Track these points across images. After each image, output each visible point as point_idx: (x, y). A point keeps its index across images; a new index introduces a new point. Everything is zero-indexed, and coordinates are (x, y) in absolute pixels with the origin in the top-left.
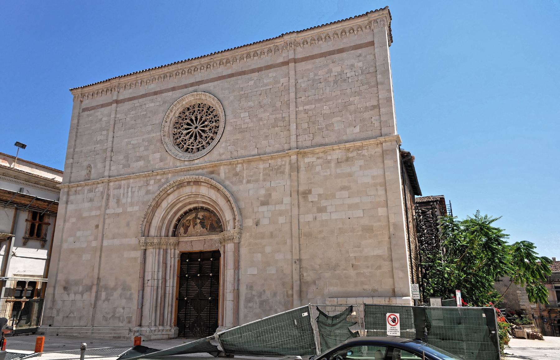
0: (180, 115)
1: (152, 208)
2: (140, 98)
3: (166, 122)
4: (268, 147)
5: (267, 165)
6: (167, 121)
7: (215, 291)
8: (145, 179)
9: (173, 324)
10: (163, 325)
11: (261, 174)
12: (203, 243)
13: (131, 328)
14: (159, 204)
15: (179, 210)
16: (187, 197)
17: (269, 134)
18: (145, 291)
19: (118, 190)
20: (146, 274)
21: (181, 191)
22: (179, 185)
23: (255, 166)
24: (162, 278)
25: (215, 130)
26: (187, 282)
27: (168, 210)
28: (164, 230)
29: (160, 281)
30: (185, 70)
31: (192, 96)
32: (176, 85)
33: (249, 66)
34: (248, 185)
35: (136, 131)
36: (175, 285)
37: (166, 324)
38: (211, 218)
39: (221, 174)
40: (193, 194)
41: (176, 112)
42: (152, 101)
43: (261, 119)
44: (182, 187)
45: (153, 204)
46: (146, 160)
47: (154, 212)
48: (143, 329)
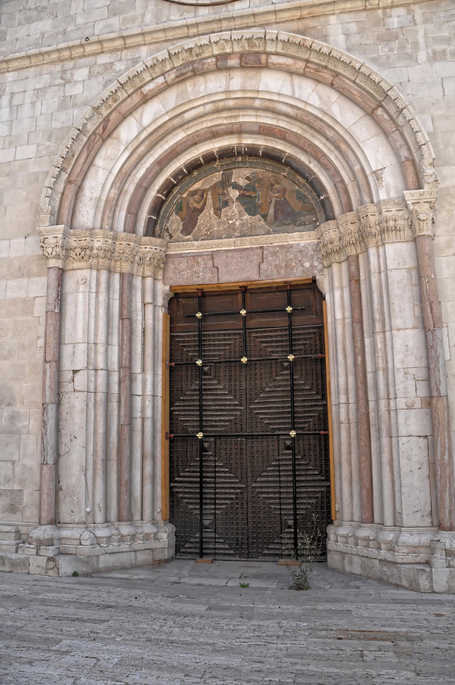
1: (85, 139)
7: (305, 412)
8: (58, 68)
9: (159, 517)
10: (130, 520)
12: (256, 259)
13: (23, 530)
14: (110, 126)
16: (209, 107)
18: (65, 407)
20: (67, 350)
21: (189, 89)
22: (184, 66)
24: (120, 367)
26: (201, 380)
27: (142, 149)
28: (123, 213)
29: (115, 378)
34: (438, 65)
36: (160, 392)
37: (137, 517)
38: (278, 183)
40: (233, 96)
45: (91, 127)
46: (60, 17)
47: (92, 153)
48: (66, 533)
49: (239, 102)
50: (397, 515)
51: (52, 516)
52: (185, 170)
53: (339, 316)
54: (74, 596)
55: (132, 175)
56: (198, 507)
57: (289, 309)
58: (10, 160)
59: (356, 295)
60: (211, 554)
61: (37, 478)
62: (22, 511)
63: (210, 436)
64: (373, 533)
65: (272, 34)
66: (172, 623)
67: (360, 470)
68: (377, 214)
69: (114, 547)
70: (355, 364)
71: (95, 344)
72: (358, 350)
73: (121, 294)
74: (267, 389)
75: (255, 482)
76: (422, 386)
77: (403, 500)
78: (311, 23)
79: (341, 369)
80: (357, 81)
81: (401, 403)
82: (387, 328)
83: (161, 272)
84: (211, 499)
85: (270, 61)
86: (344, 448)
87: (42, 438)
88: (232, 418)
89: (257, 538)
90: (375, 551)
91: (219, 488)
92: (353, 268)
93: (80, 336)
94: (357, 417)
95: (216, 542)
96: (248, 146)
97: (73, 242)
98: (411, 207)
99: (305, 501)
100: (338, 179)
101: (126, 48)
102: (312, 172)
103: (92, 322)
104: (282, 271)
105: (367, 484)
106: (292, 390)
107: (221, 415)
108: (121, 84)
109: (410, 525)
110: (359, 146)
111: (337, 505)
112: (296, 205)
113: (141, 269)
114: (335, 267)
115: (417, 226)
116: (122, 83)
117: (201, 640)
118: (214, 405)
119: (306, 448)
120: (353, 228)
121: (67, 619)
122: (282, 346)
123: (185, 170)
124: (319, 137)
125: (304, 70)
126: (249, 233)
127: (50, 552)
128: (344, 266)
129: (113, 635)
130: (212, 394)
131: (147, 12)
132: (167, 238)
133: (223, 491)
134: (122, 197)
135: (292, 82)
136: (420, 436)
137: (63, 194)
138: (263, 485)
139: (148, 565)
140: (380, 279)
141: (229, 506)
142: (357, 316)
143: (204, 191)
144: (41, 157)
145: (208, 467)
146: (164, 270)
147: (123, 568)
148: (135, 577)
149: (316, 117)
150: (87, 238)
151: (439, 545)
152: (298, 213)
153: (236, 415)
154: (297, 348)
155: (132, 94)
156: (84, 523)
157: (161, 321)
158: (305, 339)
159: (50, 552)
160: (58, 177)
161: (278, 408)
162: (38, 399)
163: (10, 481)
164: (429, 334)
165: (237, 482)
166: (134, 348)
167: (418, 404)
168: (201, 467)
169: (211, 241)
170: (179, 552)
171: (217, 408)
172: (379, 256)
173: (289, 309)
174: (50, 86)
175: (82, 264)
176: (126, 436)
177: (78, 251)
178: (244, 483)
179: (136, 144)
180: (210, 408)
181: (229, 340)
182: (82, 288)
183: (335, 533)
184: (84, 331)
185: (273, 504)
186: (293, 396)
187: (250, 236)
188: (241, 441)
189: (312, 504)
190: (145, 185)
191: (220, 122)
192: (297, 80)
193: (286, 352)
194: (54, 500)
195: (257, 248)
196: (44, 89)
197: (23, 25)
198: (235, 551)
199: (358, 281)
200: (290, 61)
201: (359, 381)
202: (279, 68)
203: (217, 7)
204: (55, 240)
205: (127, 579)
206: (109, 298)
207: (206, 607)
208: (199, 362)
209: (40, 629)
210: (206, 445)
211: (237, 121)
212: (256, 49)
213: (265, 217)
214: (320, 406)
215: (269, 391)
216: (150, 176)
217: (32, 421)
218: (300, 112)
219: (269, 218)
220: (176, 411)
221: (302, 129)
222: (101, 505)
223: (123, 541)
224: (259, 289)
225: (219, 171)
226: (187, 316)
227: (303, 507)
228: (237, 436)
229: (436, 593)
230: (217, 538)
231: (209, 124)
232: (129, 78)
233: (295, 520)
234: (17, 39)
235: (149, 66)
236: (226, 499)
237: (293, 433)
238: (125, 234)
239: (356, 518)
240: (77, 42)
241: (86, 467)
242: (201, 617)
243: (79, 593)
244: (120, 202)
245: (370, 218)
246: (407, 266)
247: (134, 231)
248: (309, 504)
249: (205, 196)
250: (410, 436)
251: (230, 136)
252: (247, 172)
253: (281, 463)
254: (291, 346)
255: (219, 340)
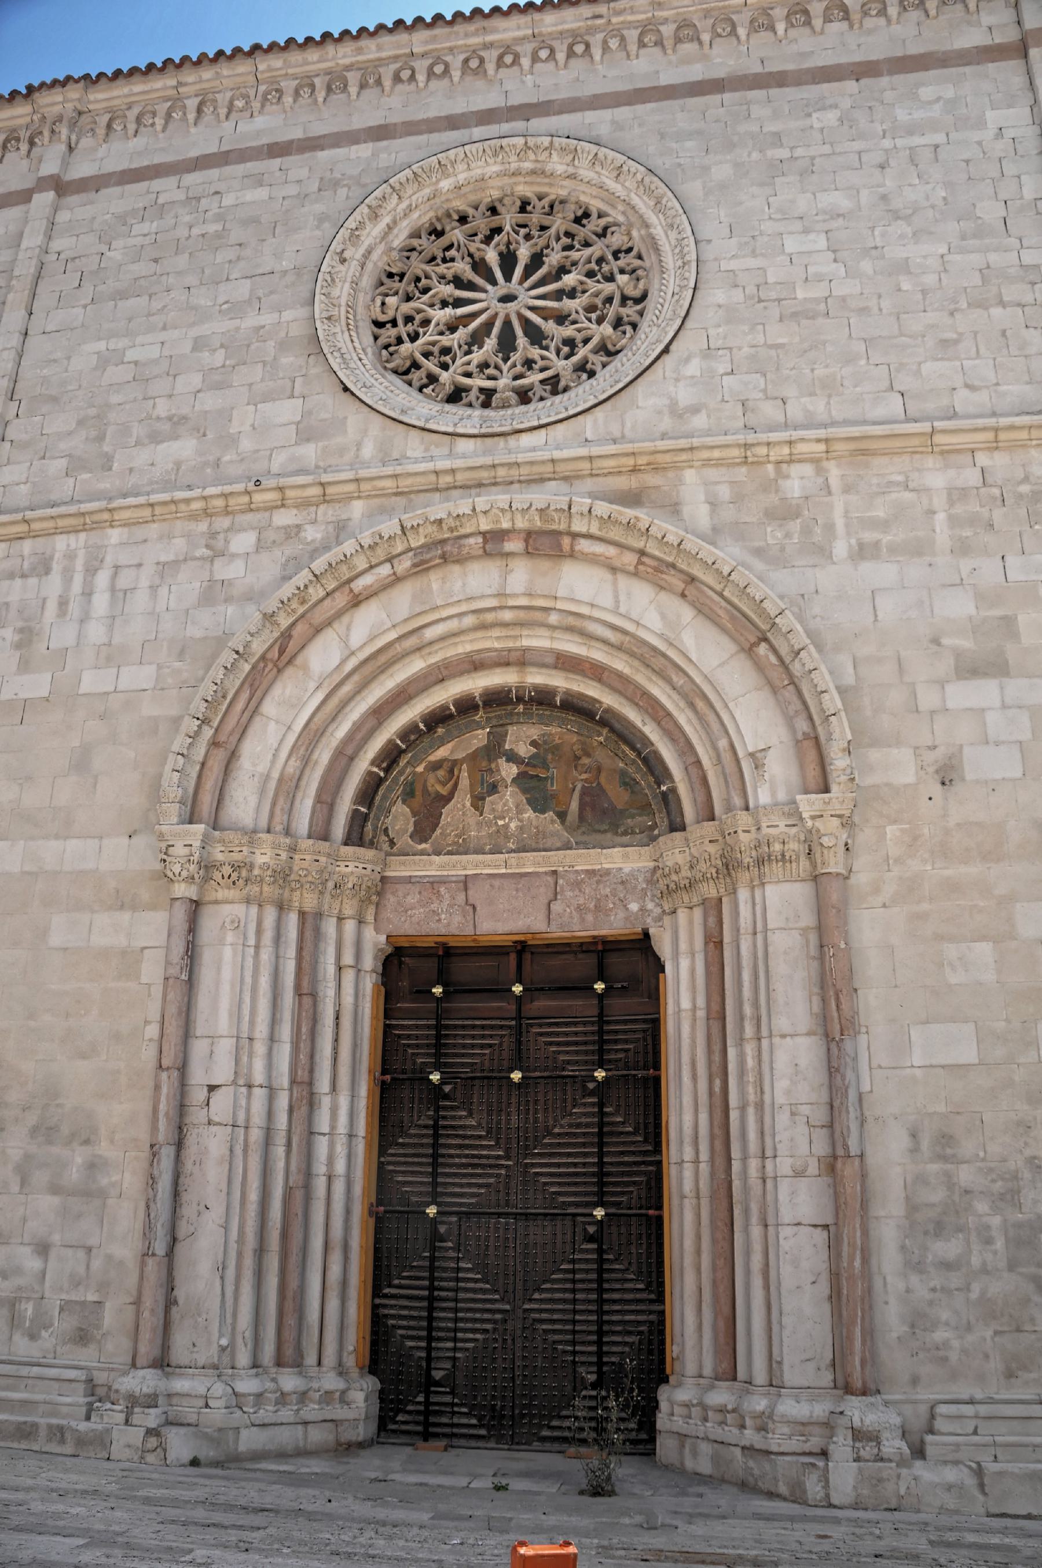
0: (415, 242)
1: (247, 667)
2: (189, 171)
3: (343, 261)
4: (964, 393)
5: (971, 477)
6: (346, 255)
7: (623, 1174)
8: (203, 526)
9: (350, 1361)
10: (298, 1363)
11: (941, 517)
12: (543, 894)
13: (100, 1377)
15: (401, 697)
16: (469, 621)
17: (961, 334)
19: (33, 581)
20: (199, 1048)
21: (435, 586)
22: (426, 547)
23: (900, 478)
24: (293, 1082)
25: (592, 357)
26: (438, 1109)
27: (347, 688)
28: (309, 802)
29: (283, 1102)
30: (448, 58)
31: (495, 154)
32: (395, 119)
33: (803, 55)
34: (866, 567)
35: (156, 305)
36: (361, 1130)
37: (311, 1359)
38: (588, 755)
39: (686, 510)
40: (511, 602)
41: (395, 222)
42: (259, 181)
43: (904, 267)
44: (445, 558)
45: (258, 647)
46: (210, 436)
47: (259, 694)
48: (181, 1385)
49: (522, 615)
50: (774, 1365)
51: (156, 1352)
52: (422, 726)
53: (686, 1004)
54: (199, 1493)
55: (327, 734)
56: (423, 1344)
57: (599, 986)
58: (106, 689)
59: (715, 969)
60: (445, 1435)
61: (133, 1280)
62: (99, 1342)
63: (451, 1213)
64: (733, 1398)
65: (582, 504)
66: (373, 1534)
67: (715, 1283)
68: (753, 829)
69: (266, 1414)
70: (711, 1093)
71: (251, 1039)
72: (716, 1067)
73: (300, 949)
74: (556, 1130)
75: (531, 1300)
76: (821, 1138)
77: (785, 1339)
78: (652, 479)
79: (687, 1100)
80: (726, 593)
81: (784, 1165)
82: (765, 1032)
83: (371, 910)
84: (448, 1330)
85: (577, 548)
86: (688, 1243)
87: (148, 1207)
88: (492, 1180)
89: (529, 1406)
90: (735, 1431)
91: (462, 1310)
92: (712, 921)
93: (224, 1024)
94: (712, 1186)
95: (454, 1413)
96: (536, 688)
97: (218, 854)
98: (810, 823)
99: (618, 1339)
100: (693, 759)
101: (325, 501)
102: (647, 741)
103: (247, 999)
104: (590, 918)
105: (726, 1310)
106: (601, 1134)
107: (472, 1175)
108: (315, 576)
109: (795, 1385)
110: (726, 706)
111: (675, 1348)
112: (618, 796)
113: (336, 905)
114: (682, 915)
115: (818, 855)
116: (318, 573)
117: (420, 1556)
118: (459, 1156)
119: (624, 1241)
120: (712, 849)
121: (196, 1524)
122: (586, 1052)
123: (422, 726)
124: (660, 682)
125: (636, 567)
126: (534, 845)
127: (152, 1418)
128: (698, 913)
129: (276, 1546)
130: (457, 1136)
131: (366, 440)
132: (386, 847)
133: (469, 1315)
134: (307, 772)
135: (615, 583)
136: (815, 1226)
137: (203, 764)
138: (543, 1306)
139: (327, 1451)
140: (755, 946)
141: (480, 1345)
142: (715, 1007)
143: (455, 763)
144: (162, 689)
145: (445, 1269)
146: (377, 905)
147: (281, 1455)
148: (304, 1470)
149: (654, 649)
150: (244, 849)
151: (843, 1421)
152: (622, 812)
153: (498, 1176)
154: (612, 1057)
155: (334, 591)
156: (215, 1367)
157: (368, 998)
158: (626, 1041)
159: (152, 1418)
160: (195, 736)
161: (575, 1165)
162: (144, 1136)
163: (79, 1284)
164: (833, 1046)
165: (496, 1300)
166: (318, 1046)
167: (813, 1168)
168: (432, 1269)
169: (464, 857)
170: (386, 1431)
171: (464, 1161)
172: (754, 904)
173: (599, 986)
174: (185, 560)
175: (232, 894)
176: (298, 1207)
177: (227, 870)
178: (508, 1303)
179: (337, 678)
180: (451, 1161)
181: (491, 1036)
182: (230, 937)
183: (669, 1400)
184: (231, 1015)
185: (560, 1342)
186: (601, 1145)
187: (534, 850)
188: (507, 1224)
189: (630, 1345)
190: (349, 751)
191: (488, 644)
192: (623, 581)
193: (593, 1064)
194: (162, 1322)
195: (546, 873)
196: (176, 563)
197: (143, 445)
198: (489, 1431)
199: (720, 944)
200: (611, 551)
201: (715, 1123)
202: (593, 560)
203: (489, 441)
204: (187, 850)
205: (290, 1473)
206: (277, 957)
207: (431, 1515)
208: (435, 1077)
209: (154, 1536)
210: (442, 1229)
211: (518, 644)
212: (555, 527)
213: (562, 816)
214: (650, 1163)
215: (559, 1134)
216: (359, 736)
217: (127, 1175)
218: (628, 638)
219: (569, 818)
220: (389, 1163)
221: (631, 666)
222: (247, 1334)
223: (284, 1404)
224: (548, 946)
225: (483, 728)
226: (418, 992)
227: (615, 1349)
228: (500, 1215)
229: (835, 1507)
230: (457, 1405)
231: (468, 648)
232: (330, 565)
233: (600, 1373)
234: (131, 470)
235: (366, 546)
236: (474, 1331)
237: (599, 1213)
238: (311, 842)
239: (708, 1371)
240: (240, 487)
241: (223, 1263)
242: (421, 1527)
243: (207, 1490)
244: (303, 783)
245: (743, 836)
246: (803, 924)
247: (325, 837)
248: (626, 1344)
249: (456, 772)
250: (799, 1224)
251: (505, 669)
252: (534, 732)
253: (577, 1266)
254: (601, 1052)
255: (473, 1037)
